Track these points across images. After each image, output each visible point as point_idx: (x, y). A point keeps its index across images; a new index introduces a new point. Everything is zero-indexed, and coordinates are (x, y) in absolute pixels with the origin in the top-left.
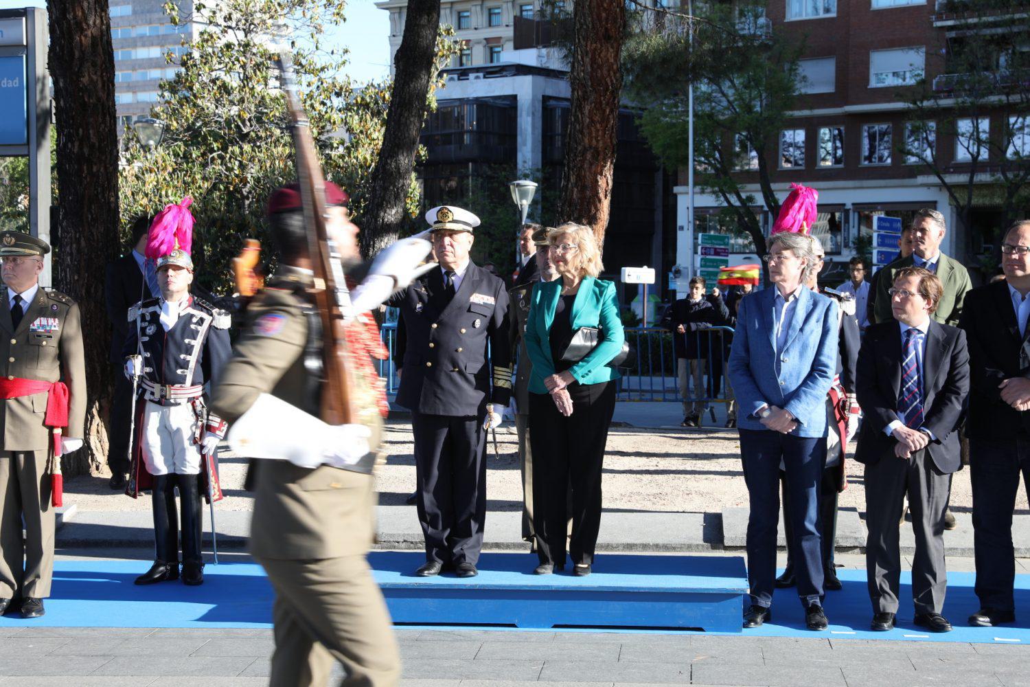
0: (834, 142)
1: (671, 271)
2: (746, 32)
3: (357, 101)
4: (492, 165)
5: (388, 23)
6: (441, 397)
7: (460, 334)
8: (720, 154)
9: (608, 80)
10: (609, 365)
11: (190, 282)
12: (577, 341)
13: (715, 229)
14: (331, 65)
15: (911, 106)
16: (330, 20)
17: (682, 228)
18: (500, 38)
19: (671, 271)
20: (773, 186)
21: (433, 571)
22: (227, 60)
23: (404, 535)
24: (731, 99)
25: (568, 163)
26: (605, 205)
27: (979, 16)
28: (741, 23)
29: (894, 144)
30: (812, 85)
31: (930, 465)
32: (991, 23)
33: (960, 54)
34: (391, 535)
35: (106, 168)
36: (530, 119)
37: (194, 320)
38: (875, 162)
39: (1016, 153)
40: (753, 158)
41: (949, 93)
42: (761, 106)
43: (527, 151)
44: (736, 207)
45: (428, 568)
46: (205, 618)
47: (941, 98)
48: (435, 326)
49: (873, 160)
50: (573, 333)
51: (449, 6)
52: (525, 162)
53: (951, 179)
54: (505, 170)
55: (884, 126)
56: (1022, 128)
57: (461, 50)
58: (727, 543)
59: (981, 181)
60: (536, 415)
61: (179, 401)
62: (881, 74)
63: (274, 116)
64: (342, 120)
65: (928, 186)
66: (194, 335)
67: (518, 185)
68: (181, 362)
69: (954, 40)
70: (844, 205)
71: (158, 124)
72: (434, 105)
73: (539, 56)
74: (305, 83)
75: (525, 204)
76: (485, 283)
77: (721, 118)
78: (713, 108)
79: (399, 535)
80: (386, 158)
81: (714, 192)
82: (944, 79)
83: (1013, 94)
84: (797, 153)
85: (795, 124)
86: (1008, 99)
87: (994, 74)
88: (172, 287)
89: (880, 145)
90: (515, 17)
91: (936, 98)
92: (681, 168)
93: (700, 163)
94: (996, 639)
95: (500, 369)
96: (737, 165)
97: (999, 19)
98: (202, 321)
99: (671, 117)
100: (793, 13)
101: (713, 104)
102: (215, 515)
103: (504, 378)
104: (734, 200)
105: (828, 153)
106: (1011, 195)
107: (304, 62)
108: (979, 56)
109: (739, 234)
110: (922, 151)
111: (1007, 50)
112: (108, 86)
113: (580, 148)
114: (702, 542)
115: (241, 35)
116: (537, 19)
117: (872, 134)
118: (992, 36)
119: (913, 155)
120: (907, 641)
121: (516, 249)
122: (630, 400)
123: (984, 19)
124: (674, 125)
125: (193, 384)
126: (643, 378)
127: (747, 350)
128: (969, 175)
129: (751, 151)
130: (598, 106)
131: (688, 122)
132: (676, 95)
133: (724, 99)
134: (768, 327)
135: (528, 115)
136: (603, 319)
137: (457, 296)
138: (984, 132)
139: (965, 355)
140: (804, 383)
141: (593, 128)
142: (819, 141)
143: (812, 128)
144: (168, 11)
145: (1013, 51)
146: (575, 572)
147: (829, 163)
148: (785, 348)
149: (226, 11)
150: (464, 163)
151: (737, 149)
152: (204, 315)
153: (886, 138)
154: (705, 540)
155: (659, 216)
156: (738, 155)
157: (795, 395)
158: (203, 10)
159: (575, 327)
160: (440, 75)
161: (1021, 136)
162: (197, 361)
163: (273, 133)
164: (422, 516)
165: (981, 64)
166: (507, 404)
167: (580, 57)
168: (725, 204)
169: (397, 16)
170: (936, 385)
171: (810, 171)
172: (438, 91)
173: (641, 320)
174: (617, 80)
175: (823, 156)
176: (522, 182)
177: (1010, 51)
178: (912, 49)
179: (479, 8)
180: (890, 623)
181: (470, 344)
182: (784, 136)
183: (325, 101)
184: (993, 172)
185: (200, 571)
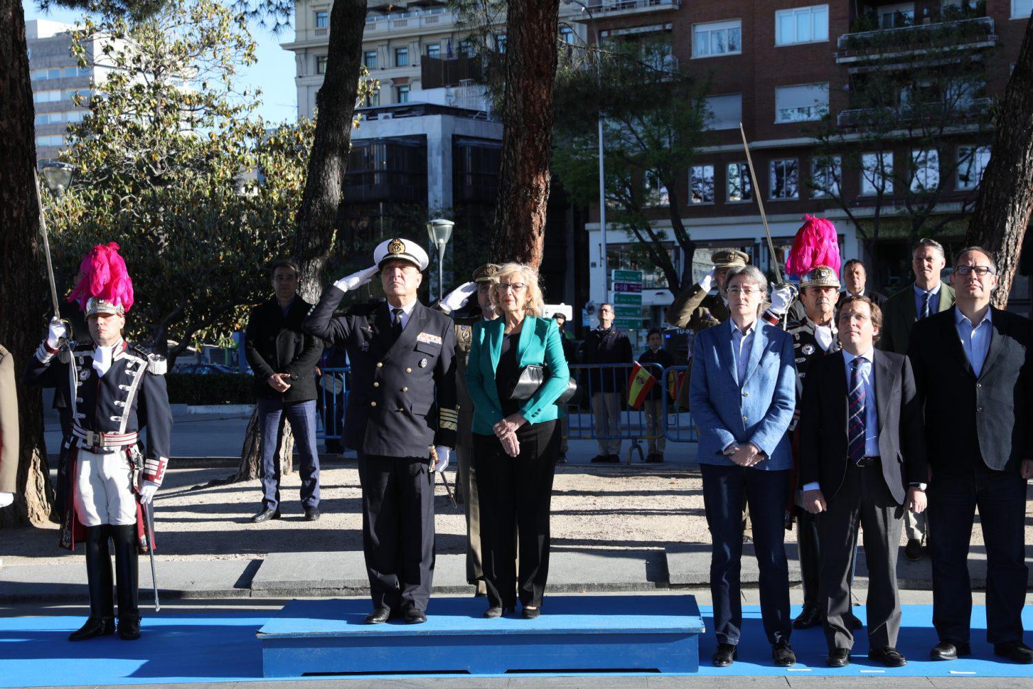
0: (742, 178)
1: (584, 308)
3: (270, 141)
4: (404, 205)
5: (294, 63)
6: (386, 437)
7: (405, 374)
8: (630, 191)
9: (541, 116)
10: (557, 402)
11: (122, 327)
12: (525, 379)
14: (244, 105)
15: (817, 141)
16: (242, 61)
17: (594, 265)
18: (407, 78)
19: (584, 308)
20: (684, 222)
21: (382, 619)
22: (137, 102)
23: (344, 582)
24: (641, 136)
25: (502, 200)
26: (539, 241)
27: (881, 53)
28: (648, 61)
29: (801, 178)
30: (720, 121)
32: (892, 59)
33: (863, 90)
34: (331, 582)
35: (26, 213)
36: (440, 158)
37: (129, 365)
38: (783, 197)
39: (920, 186)
40: (663, 194)
41: (854, 128)
42: (670, 143)
44: (648, 243)
45: (377, 616)
46: (138, 674)
47: (846, 133)
48: (380, 365)
49: (781, 195)
51: (386, 43)
52: (436, 201)
53: (856, 213)
55: (791, 161)
56: (924, 162)
58: (672, 581)
59: (887, 214)
60: (479, 454)
61: (112, 449)
62: (787, 110)
63: (186, 158)
64: (256, 161)
66: (128, 380)
67: (435, 224)
68: (115, 409)
69: (857, 76)
70: (754, 239)
71: (67, 168)
73: (447, 96)
74: (217, 125)
76: (432, 324)
77: (631, 154)
78: (623, 145)
79: (339, 581)
80: (311, 199)
81: (625, 229)
82: (848, 115)
83: (916, 128)
84: (707, 188)
85: (703, 160)
86: (911, 135)
87: (896, 109)
88: (104, 335)
89: (787, 180)
90: (423, 57)
92: (592, 205)
93: (611, 199)
94: (952, 672)
95: (446, 410)
96: (647, 201)
97: (899, 55)
98: (136, 366)
99: (581, 155)
100: (699, 50)
101: (623, 141)
102: (156, 569)
103: (449, 421)
104: (646, 237)
105: (736, 188)
107: (215, 103)
108: (882, 91)
109: (650, 270)
110: (828, 185)
111: (908, 85)
112: (28, 129)
113: (513, 186)
114: (646, 581)
115: (151, 78)
116: (445, 58)
117: (794, 172)
118: (894, 72)
119: (820, 189)
120: (863, 676)
121: (428, 288)
123: (885, 55)
124: (584, 162)
125: (127, 432)
127: (707, 386)
128: (875, 208)
129: (661, 187)
131: (598, 159)
133: (633, 136)
134: (727, 360)
135: (438, 154)
136: (548, 356)
137: (404, 334)
138: (888, 166)
140: (768, 415)
141: (526, 166)
142: (728, 176)
143: (720, 163)
144: (76, 53)
145: (914, 87)
146: (525, 615)
147: (738, 199)
148: (746, 382)
149: (134, 54)
150: (375, 203)
151: (648, 186)
152: (140, 361)
153: (793, 173)
154: (649, 578)
155: (570, 254)
157: (760, 426)
158: (111, 53)
159: (522, 365)
161: (924, 169)
162: (132, 407)
163: (185, 175)
165: (883, 100)
167: (511, 94)
168: (637, 240)
169: (303, 57)
171: (719, 207)
174: (549, 117)
175: (731, 191)
176: (440, 221)
177: (911, 87)
178: (817, 85)
179: (416, 45)
180: (845, 659)
181: (417, 387)
182: (693, 171)
183: (238, 142)
184: (898, 205)
185: (137, 623)
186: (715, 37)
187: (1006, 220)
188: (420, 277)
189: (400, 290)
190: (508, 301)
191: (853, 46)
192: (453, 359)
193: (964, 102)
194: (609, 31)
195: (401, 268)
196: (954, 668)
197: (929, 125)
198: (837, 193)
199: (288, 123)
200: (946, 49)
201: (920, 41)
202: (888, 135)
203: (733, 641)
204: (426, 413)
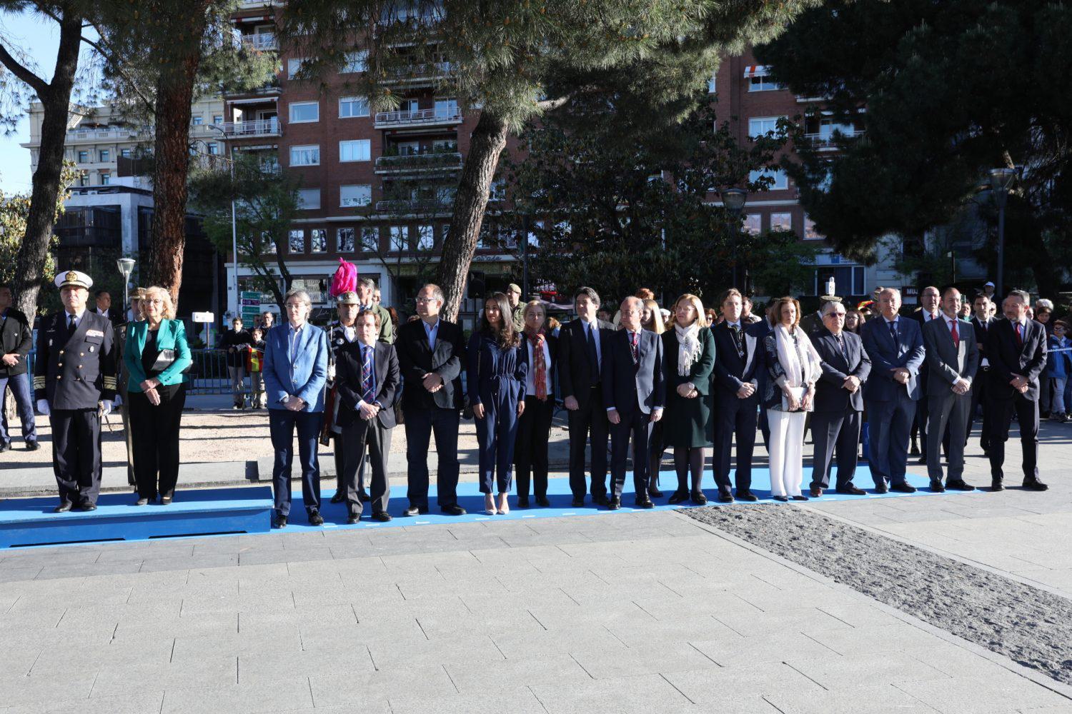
2: (266, 172)
12: (161, 358)
13: (251, 288)
17: (230, 288)
20: (286, 264)
26: (179, 274)
29: (355, 239)
30: (306, 204)
31: (380, 425)
36: (130, 220)
38: (345, 251)
39: (423, 247)
41: (385, 212)
43: (129, 239)
45: (63, 507)
48: (62, 352)
50: (158, 353)
53: (388, 261)
54: (114, 251)
55: (349, 230)
56: (425, 233)
57: (81, 176)
58: (261, 478)
60: (135, 407)
65: (376, 264)
67: (123, 261)
69: (387, 182)
72: (63, 210)
75: (128, 273)
76: (96, 322)
77: (253, 222)
85: (297, 227)
91: (378, 214)
92: (228, 252)
93: (240, 249)
103: (111, 384)
106: (421, 270)
109: (266, 292)
116: (133, 158)
117: (345, 237)
122: (199, 394)
123: (403, 171)
126: (207, 380)
127: (273, 363)
130: (172, 211)
132: (224, 208)
134: (285, 347)
136: (177, 344)
137: (77, 331)
139: (396, 361)
140: (310, 380)
143: (308, 229)
146: (162, 503)
147: (318, 251)
150: (86, 247)
154: (247, 477)
155: (216, 281)
156: (264, 244)
157: (305, 388)
159: (160, 350)
160: (67, 191)
164: (57, 473)
166: (113, 399)
168: (257, 274)
170: (382, 378)
171: (307, 255)
172: (64, 202)
173: (206, 345)
176: (125, 259)
179: (114, 149)
181: (88, 363)
184: (411, 257)
186: (304, 154)
187: (457, 267)
188: (87, 293)
189: (75, 304)
190: (150, 310)
191: (385, 164)
192: (112, 346)
193: (447, 200)
194: (239, 147)
195: (75, 290)
196: (415, 518)
197: (428, 212)
198: (376, 249)
199: (21, 195)
200: (436, 169)
201: (422, 164)
202: (404, 216)
203: (286, 513)
204: (94, 381)
